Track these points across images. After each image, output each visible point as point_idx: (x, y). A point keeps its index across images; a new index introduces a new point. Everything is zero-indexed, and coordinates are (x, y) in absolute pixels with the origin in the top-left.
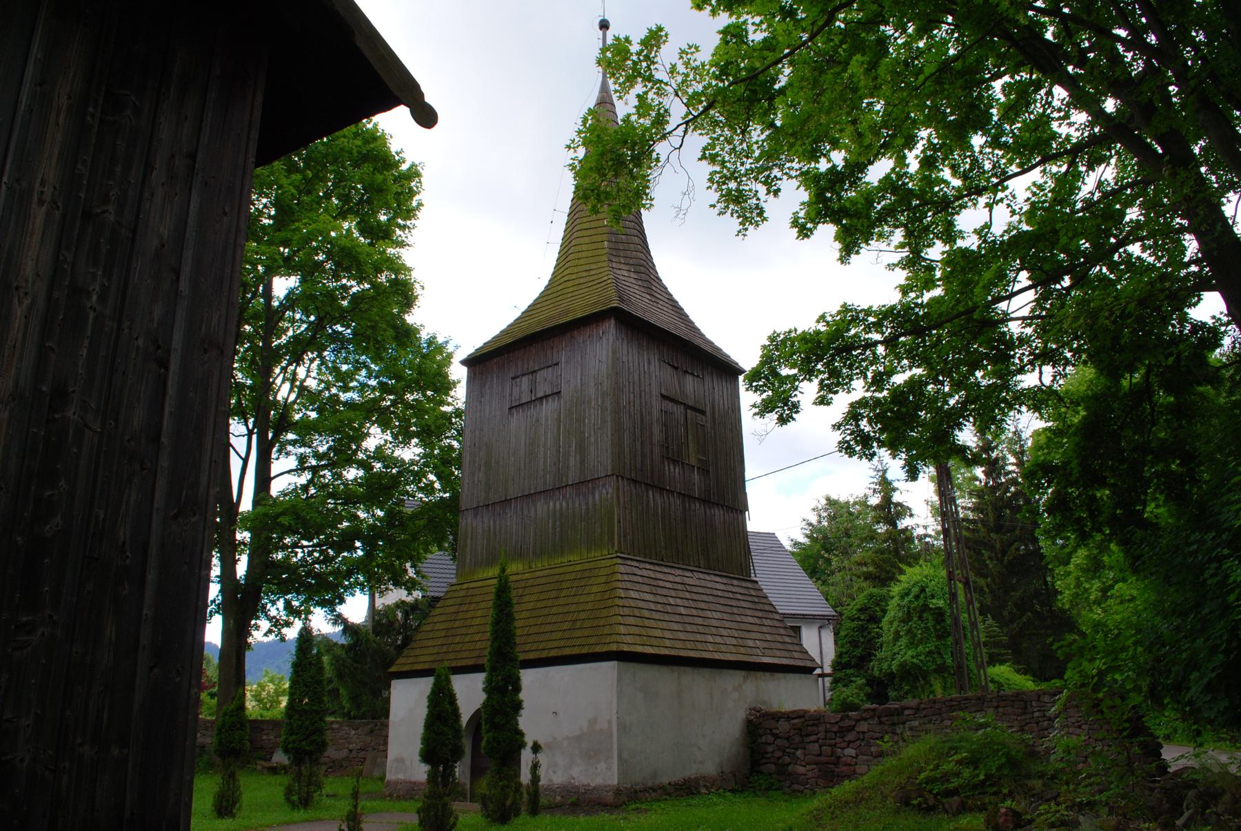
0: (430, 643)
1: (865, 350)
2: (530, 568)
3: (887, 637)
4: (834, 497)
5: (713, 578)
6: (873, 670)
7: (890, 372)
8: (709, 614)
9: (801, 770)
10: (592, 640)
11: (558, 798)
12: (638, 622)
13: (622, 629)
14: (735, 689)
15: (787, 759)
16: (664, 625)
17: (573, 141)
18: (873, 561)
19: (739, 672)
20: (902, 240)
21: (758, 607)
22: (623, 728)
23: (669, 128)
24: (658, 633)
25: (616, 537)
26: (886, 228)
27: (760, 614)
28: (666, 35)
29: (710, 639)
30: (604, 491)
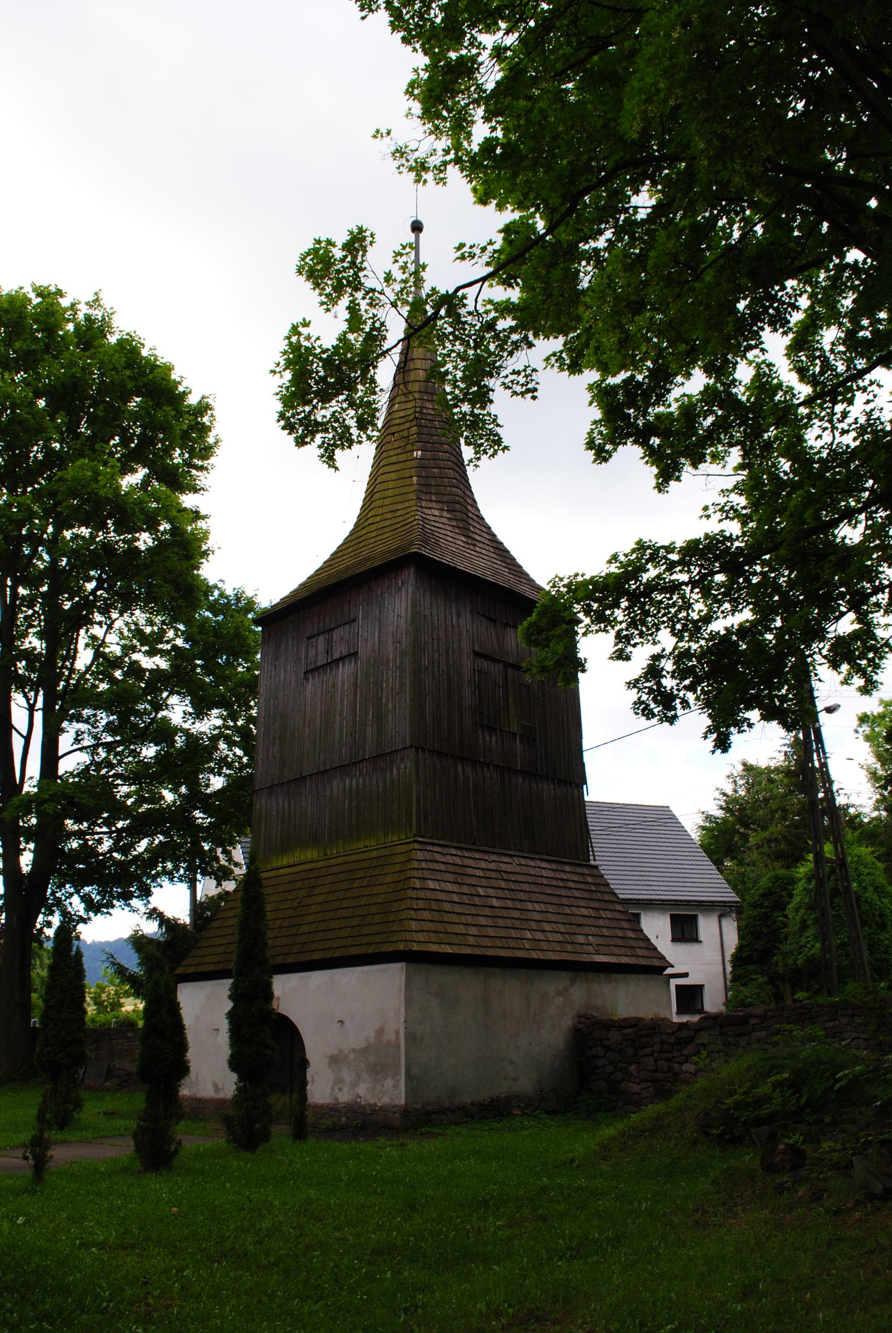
0: (218, 941)
1: (672, 594)
2: (326, 854)
3: (793, 927)
4: (752, 761)
5: (539, 863)
6: (776, 965)
7: (707, 619)
8: (529, 906)
9: (635, 1088)
10: (379, 939)
11: (344, 1119)
12: (436, 916)
13: (414, 925)
14: (559, 993)
15: (619, 1075)
16: (470, 920)
17: (278, 364)
18: (784, 837)
19: (564, 973)
20: (740, 460)
21: (595, 896)
22: (412, 1039)
23: (386, 345)
24: (460, 929)
25: (414, 818)
26: (720, 448)
27: (597, 905)
28: (372, 235)
29: (528, 935)
30: (402, 766)
